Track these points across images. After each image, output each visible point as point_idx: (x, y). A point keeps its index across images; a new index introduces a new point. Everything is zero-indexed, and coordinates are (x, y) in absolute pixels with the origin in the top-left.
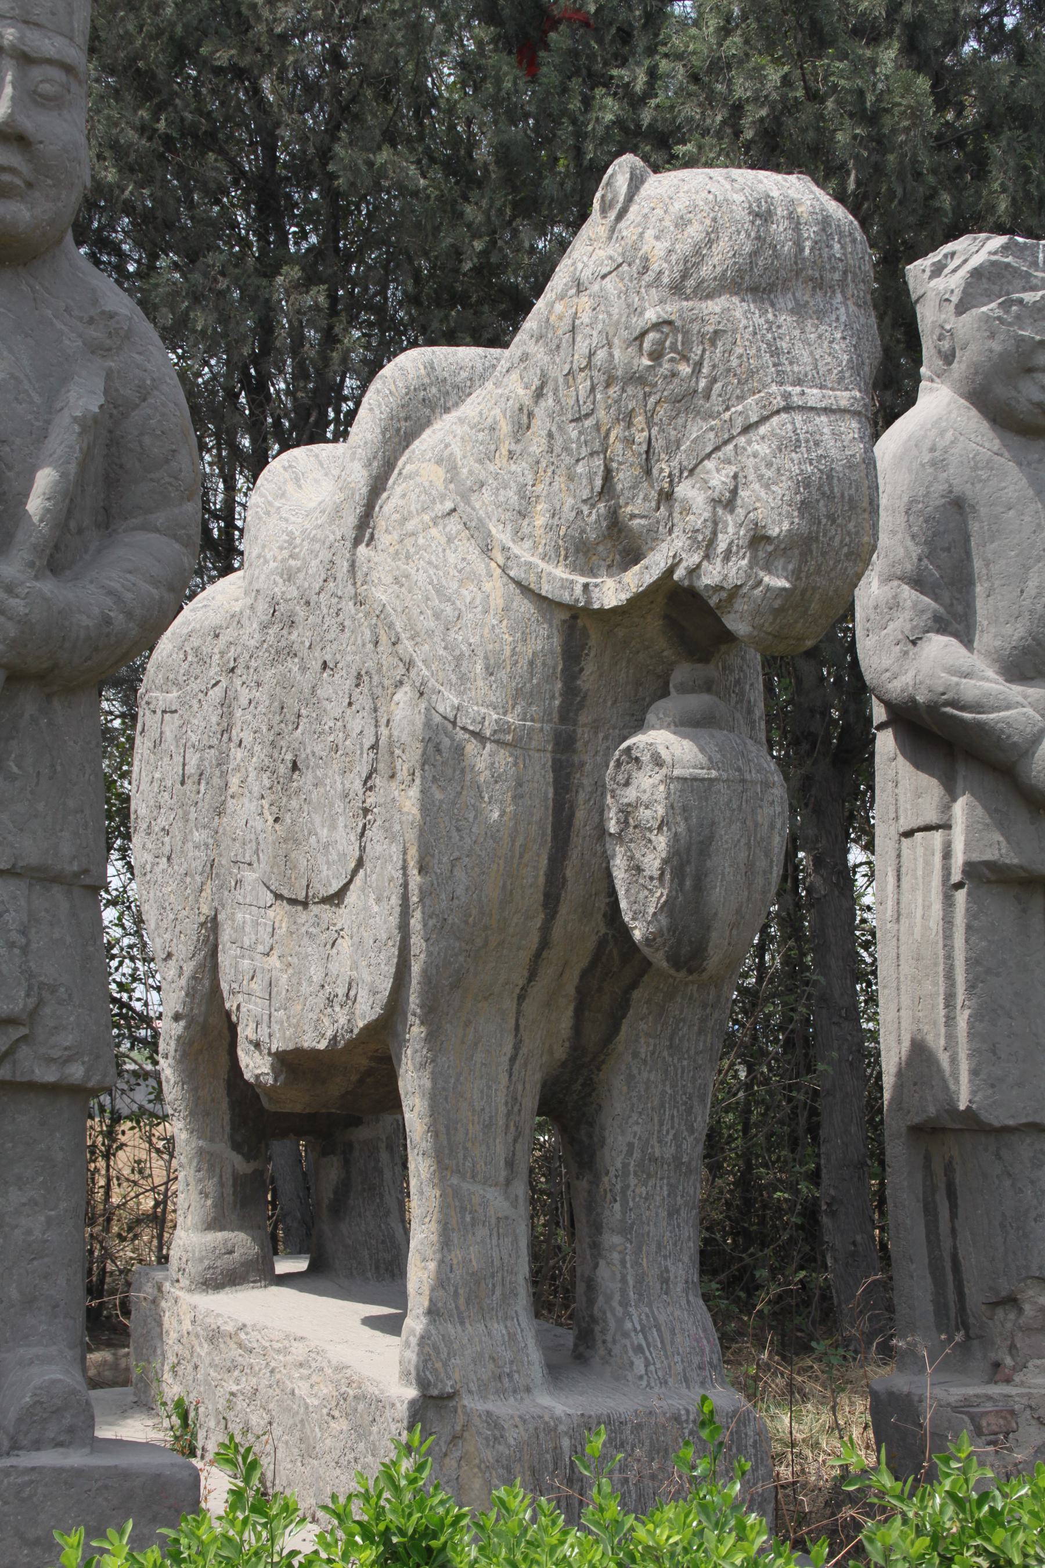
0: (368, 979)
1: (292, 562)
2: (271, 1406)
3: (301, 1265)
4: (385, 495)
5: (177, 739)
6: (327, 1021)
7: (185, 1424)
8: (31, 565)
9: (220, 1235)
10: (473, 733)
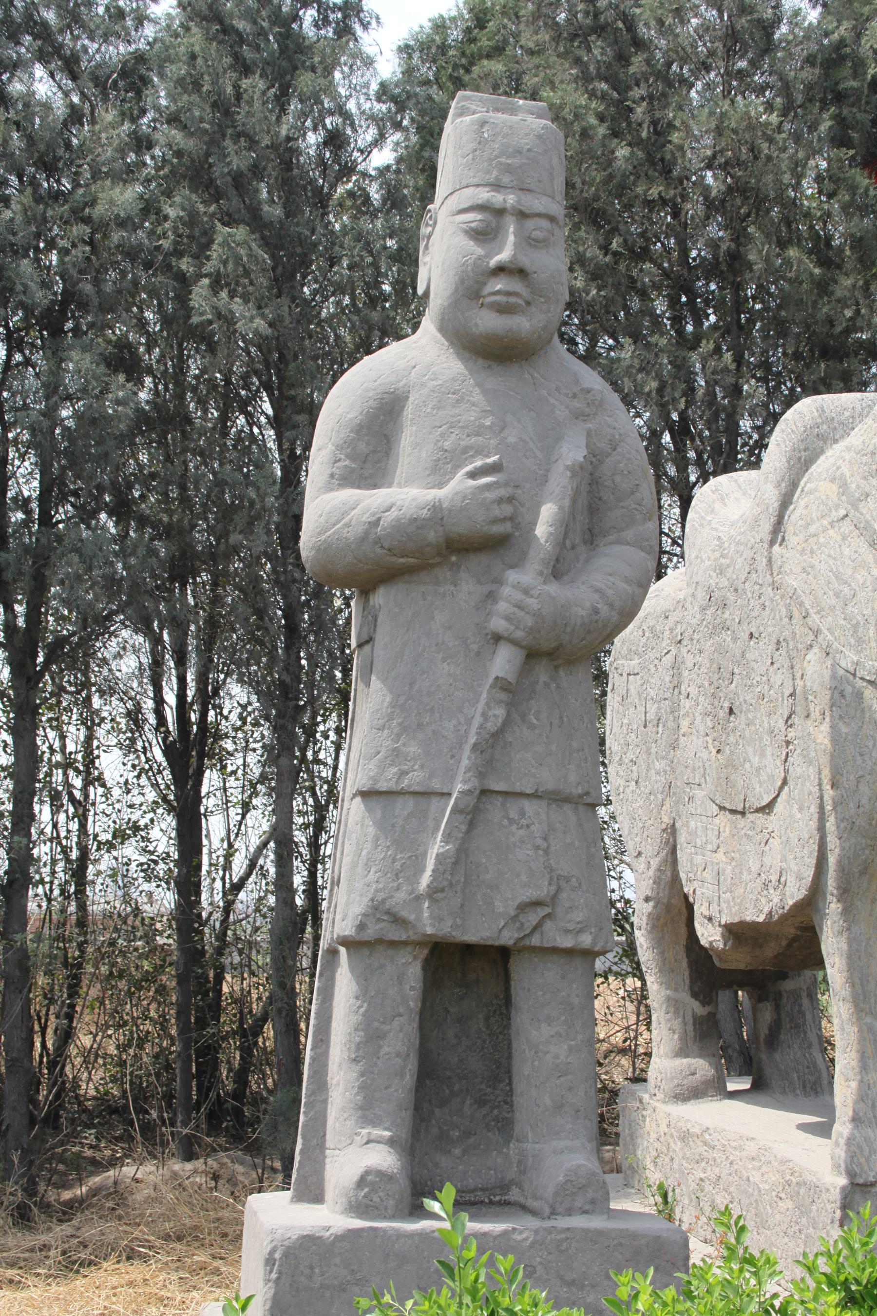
0: (795, 868)
1: (722, 561)
2: (732, 1189)
3: (744, 1084)
4: (792, 507)
5: (639, 694)
6: (763, 900)
7: (666, 1202)
8: (541, 573)
9: (685, 1061)
10: (869, 682)
